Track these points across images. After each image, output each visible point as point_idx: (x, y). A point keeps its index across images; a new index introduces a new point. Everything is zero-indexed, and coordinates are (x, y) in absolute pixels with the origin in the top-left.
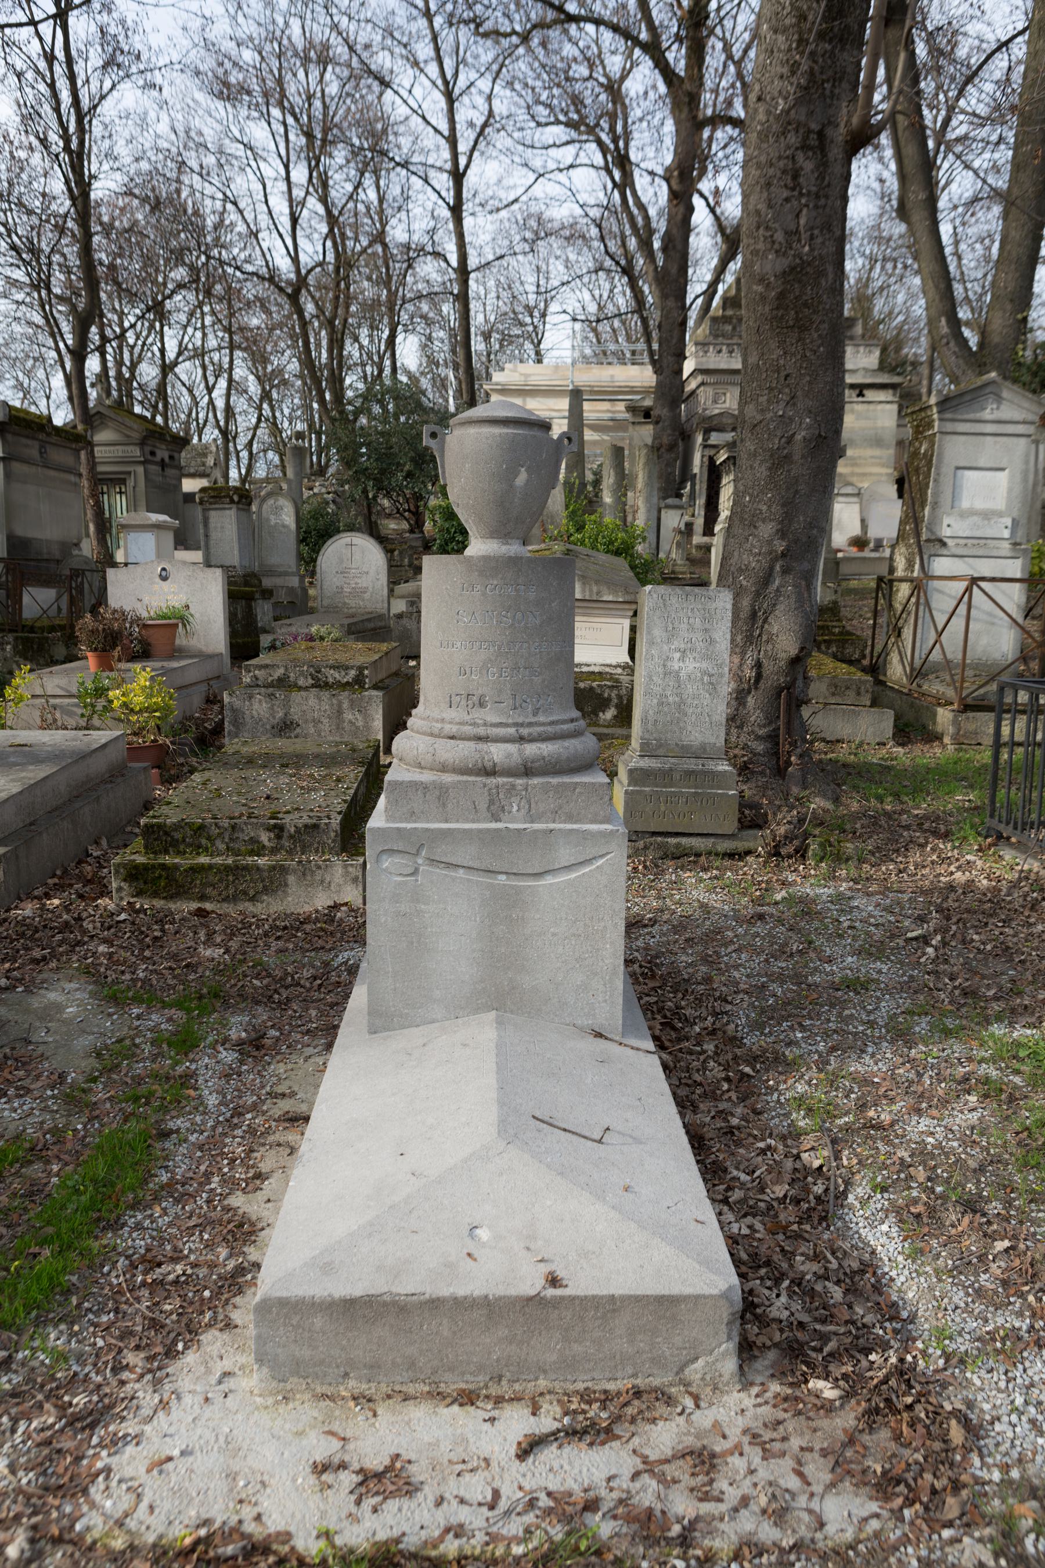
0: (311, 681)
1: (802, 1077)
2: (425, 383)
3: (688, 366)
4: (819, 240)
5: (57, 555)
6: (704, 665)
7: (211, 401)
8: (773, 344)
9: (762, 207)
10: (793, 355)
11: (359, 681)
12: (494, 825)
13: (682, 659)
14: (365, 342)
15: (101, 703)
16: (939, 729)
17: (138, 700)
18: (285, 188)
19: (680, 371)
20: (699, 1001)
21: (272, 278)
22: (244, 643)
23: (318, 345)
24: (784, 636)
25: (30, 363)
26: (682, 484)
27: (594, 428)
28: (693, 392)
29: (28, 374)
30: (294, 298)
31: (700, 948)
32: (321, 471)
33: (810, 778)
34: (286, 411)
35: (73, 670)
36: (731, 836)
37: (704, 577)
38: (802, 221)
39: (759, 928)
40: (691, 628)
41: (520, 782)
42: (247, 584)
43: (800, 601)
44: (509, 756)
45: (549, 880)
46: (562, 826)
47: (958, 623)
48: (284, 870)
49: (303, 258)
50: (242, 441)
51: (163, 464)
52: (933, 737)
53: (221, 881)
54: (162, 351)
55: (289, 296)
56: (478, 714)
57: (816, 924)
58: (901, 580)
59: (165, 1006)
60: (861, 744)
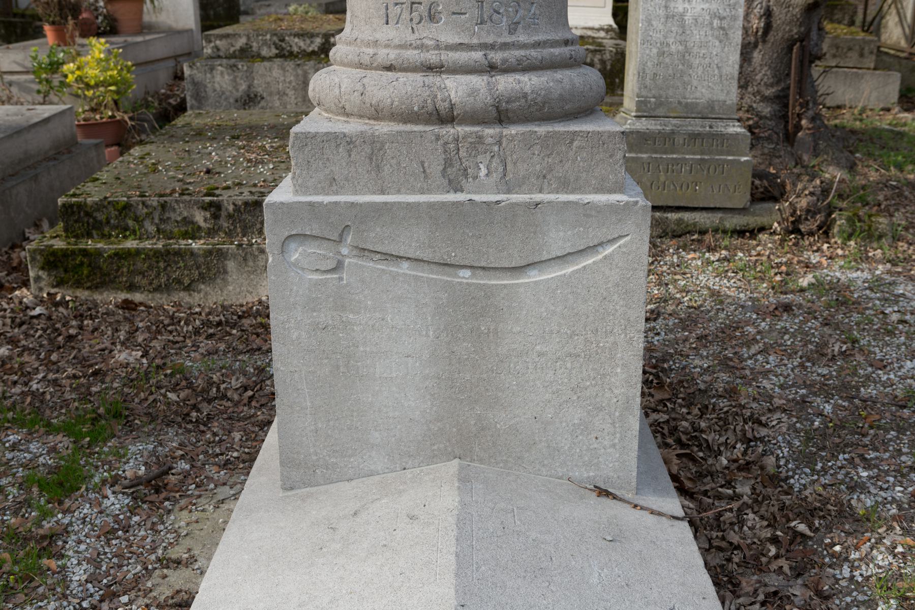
1: (880, 541)
12: (452, 197)
15: (56, 80)
17: (92, 73)
20: (724, 423)
31: (715, 348)
33: (822, 144)
36: (743, 211)
39: (785, 322)
41: (490, 132)
44: (473, 92)
45: (534, 276)
46: (552, 197)
48: (221, 255)
53: (150, 268)
56: (429, 33)
57: (856, 317)
59: (50, 429)
60: (863, 110)
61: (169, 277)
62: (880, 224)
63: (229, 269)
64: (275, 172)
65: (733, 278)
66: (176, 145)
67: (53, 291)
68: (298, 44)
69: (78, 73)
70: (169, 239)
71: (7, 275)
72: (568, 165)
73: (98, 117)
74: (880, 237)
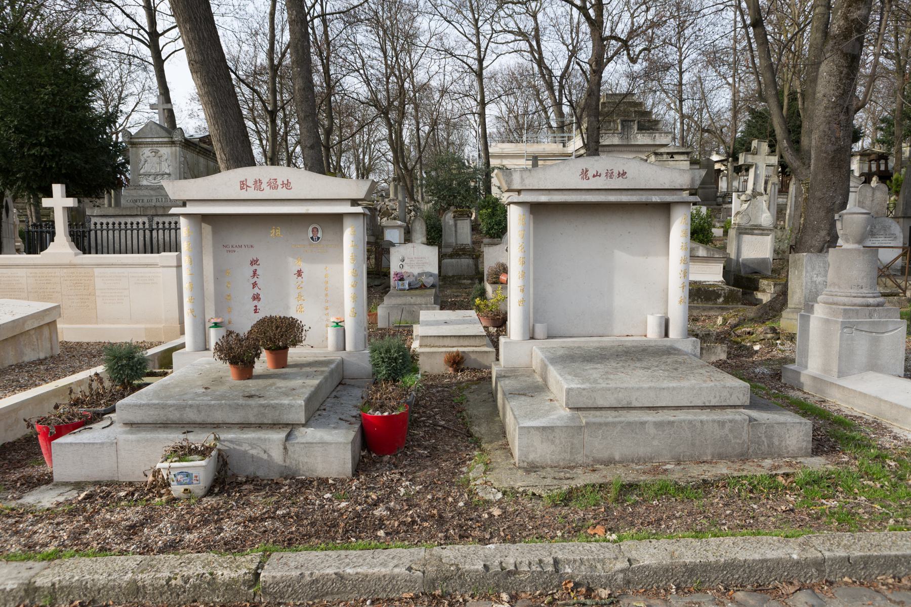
9: (826, 130)
40: (820, 267)
56: (861, 291)
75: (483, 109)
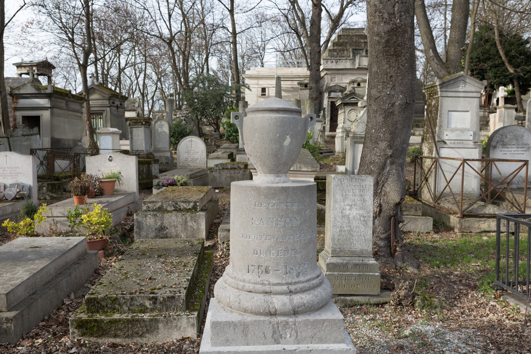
0: (173, 208)
2: (219, 74)
3: (322, 68)
4: (404, 17)
5: (72, 145)
6: (361, 212)
7: (138, 83)
8: (384, 62)
10: (394, 67)
11: (195, 208)
13: (350, 209)
14: (197, 60)
16: (452, 225)
18: (166, 4)
19: (319, 69)
21: (160, 37)
22: (145, 184)
23: (179, 60)
24: (393, 193)
25: (69, 68)
26: (319, 111)
27: (285, 91)
28: (323, 77)
29: (68, 72)
30: (170, 44)
32: (180, 108)
34: (167, 85)
35: (67, 203)
36: (378, 296)
37: (332, 149)
38: (396, 9)
41: (291, 320)
42: (148, 158)
43: (399, 176)
47: (458, 177)
48: (157, 321)
49: (173, 29)
50: (150, 97)
51: (117, 107)
52: (450, 229)
53: (125, 327)
54: (119, 64)
55: (168, 43)
56: (265, 277)
58: (427, 158)
61: (133, 331)
62: (435, 301)
63: (160, 327)
64: (179, 278)
65: (377, 330)
66: (134, 261)
67: (79, 338)
68: (183, 205)
69: (88, 219)
70: (134, 313)
71: (57, 327)
72: (322, 333)
73: (95, 238)
74: (436, 308)
75: (235, 37)
